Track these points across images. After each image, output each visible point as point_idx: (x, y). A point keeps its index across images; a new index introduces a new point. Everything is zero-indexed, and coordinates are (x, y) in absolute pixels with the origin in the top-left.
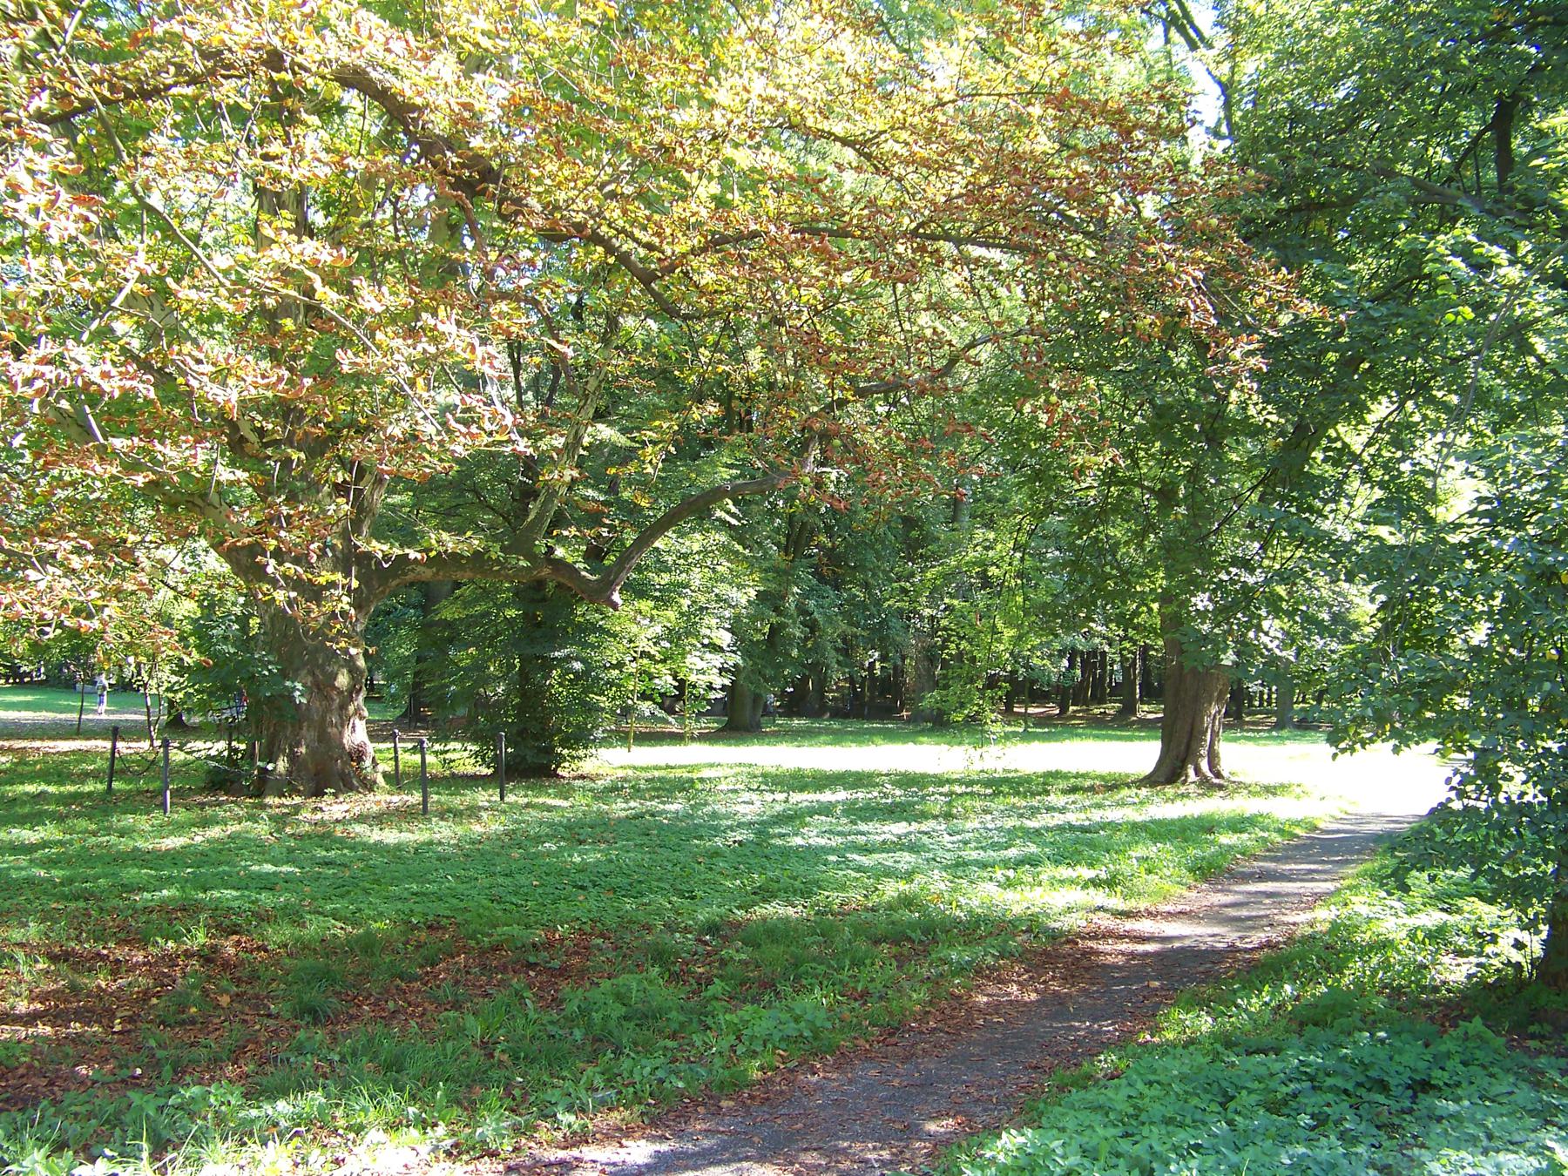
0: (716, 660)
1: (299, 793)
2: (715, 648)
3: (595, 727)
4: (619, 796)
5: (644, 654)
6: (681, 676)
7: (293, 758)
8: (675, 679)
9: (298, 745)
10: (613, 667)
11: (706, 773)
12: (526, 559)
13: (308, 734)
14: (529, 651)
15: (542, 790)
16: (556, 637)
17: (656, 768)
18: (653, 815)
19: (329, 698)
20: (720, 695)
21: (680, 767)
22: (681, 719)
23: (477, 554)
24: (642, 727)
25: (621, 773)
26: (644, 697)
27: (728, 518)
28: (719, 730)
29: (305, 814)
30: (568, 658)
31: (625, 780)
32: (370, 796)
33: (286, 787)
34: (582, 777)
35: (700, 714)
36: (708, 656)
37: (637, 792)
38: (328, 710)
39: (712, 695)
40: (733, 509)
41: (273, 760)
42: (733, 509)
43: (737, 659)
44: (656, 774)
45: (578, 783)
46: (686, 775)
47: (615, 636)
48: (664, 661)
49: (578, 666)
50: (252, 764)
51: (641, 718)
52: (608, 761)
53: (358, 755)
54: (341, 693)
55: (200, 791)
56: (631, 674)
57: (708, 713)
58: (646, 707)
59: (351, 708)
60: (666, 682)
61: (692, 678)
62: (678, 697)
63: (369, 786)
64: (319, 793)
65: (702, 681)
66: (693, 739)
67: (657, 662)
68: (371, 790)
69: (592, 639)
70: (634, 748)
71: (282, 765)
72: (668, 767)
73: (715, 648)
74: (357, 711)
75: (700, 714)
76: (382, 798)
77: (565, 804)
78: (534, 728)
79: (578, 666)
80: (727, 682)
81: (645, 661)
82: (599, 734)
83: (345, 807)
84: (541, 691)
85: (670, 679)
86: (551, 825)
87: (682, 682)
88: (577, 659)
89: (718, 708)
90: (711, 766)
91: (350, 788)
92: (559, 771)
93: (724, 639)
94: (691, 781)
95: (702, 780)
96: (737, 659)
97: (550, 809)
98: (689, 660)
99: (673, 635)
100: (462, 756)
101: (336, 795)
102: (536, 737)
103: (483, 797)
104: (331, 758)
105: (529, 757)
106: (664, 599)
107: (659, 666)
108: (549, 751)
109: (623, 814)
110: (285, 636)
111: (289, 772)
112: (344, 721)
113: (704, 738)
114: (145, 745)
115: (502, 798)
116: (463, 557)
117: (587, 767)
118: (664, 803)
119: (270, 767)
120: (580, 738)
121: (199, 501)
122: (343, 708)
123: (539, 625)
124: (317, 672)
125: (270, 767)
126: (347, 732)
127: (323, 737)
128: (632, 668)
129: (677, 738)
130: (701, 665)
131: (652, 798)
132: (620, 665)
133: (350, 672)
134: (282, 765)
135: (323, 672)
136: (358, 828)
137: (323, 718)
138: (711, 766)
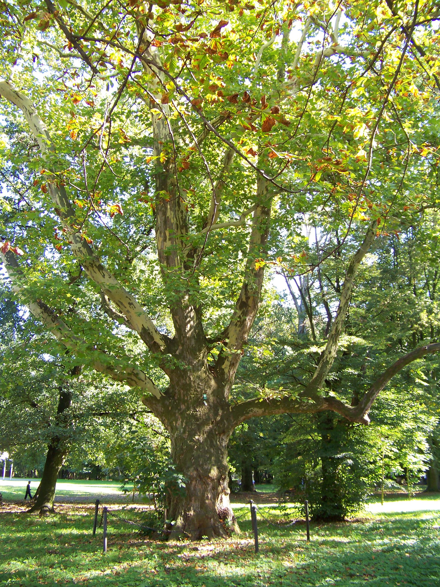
0: (421, 457)
1: (188, 537)
2: (420, 451)
3: (363, 494)
4: (377, 534)
5: (386, 456)
6: (405, 466)
7: (186, 518)
8: (402, 468)
9: (189, 510)
10: (371, 463)
11: (424, 517)
12: (313, 399)
13: (195, 504)
14: (324, 455)
15: (333, 531)
16: (338, 448)
17: (397, 514)
18: (398, 549)
19: (206, 484)
20: (424, 475)
21: (410, 513)
22: (406, 487)
23: (285, 399)
24: (387, 492)
25: (378, 518)
26: (387, 477)
27: (423, 383)
28: (425, 491)
29: (186, 553)
30: (344, 458)
31: (381, 522)
32: (229, 540)
33: (180, 534)
34: (357, 521)
35: (415, 484)
36: (417, 455)
37: (388, 532)
38: (205, 490)
39: (421, 475)
40: (425, 378)
41: (175, 519)
42: (425, 378)
43: (431, 457)
44: (398, 517)
45: (355, 525)
46: (414, 518)
47: (370, 446)
48: (395, 459)
49: (350, 462)
50: (163, 522)
51: (387, 487)
52: (372, 511)
53: (224, 515)
54: (212, 480)
55: (136, 536)
56: (381, 466)
57: (419, 484)
58: (389, 482)
59: (220, 489)
60: (397, 469)
61: (411, 467)
62: (404, 477)
63: (229, 532)
64: (199, 538)
65: (415, 468)
66: (412, 497)
67: (392, 460)
68: (230, 536)
69: (357, 447)
70: (384, 503)
71: (180, 521)
72: (403, 513)
73: (420, 451)
74: (223, 490)
75: (415, 484)
76: (242, 540)
77: (345, 540)
78: (331, 495)
79: (350, 462)
80: (428, 469)
81: (387, 460)
82: (365, 497)
83: (212, 547)
84: (334, 476)
85: (399, 468)
86: (333, 559)
87: (405, 469)
88: (350, 458)
89: (424, 481)
90: (425, 512)
91: (218, 535)
92: (346, 518)
93: (425, 446)
94: (417, 522)
95: (423, 521)
96: (431, 457)
97: (336, 544)
98: (408, 458)
99: (399, 444)
100: (293, 510)
101: (209, 539)
102: (332, 500)
103: (299, 537)
104: (207, 518)
105: (329, 511)
106: (394, 423)
107: (393, 462)
108: (339, 507)
109: (380, 548)
110: (182, 449)
111: (184, 526)
112: (216, 496)
113: (418, 496)
114: (153, 507)
115: (308, 538)
116: (278, 401)
117: (360, 515)
118: (404, 539)
119: (173, 523)
120: (356, 499)
121: (134, 378)
122: (215, 488)
123: (330, 441)
124: (199, 469)
125: (173, 523)
126: (218, 503)
127: (203, 504)
128: (380, 463)
129: (405, 496)
130: (414, 460)
131: (396, 535)
132: (374, 462)
133: (218, 468)
134: (180, 521)
135: (203, 469)
136: (212, 564)
137: (203, 495)
138: (425, 512)
